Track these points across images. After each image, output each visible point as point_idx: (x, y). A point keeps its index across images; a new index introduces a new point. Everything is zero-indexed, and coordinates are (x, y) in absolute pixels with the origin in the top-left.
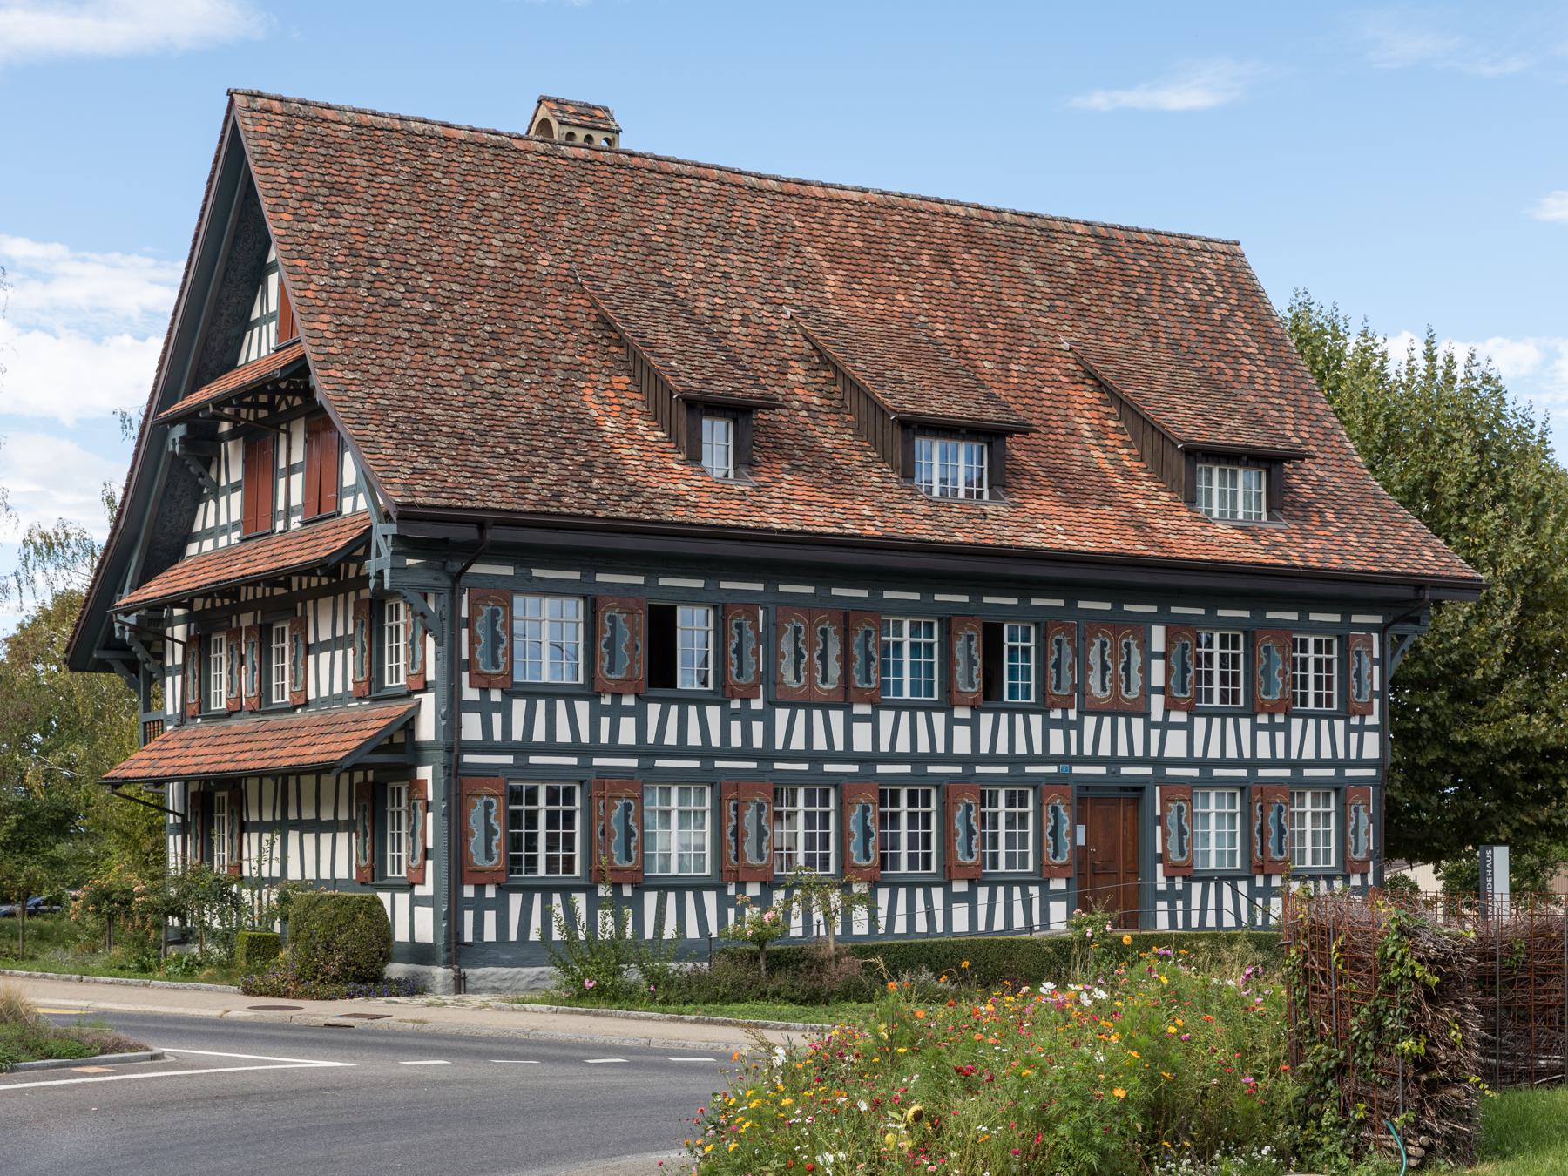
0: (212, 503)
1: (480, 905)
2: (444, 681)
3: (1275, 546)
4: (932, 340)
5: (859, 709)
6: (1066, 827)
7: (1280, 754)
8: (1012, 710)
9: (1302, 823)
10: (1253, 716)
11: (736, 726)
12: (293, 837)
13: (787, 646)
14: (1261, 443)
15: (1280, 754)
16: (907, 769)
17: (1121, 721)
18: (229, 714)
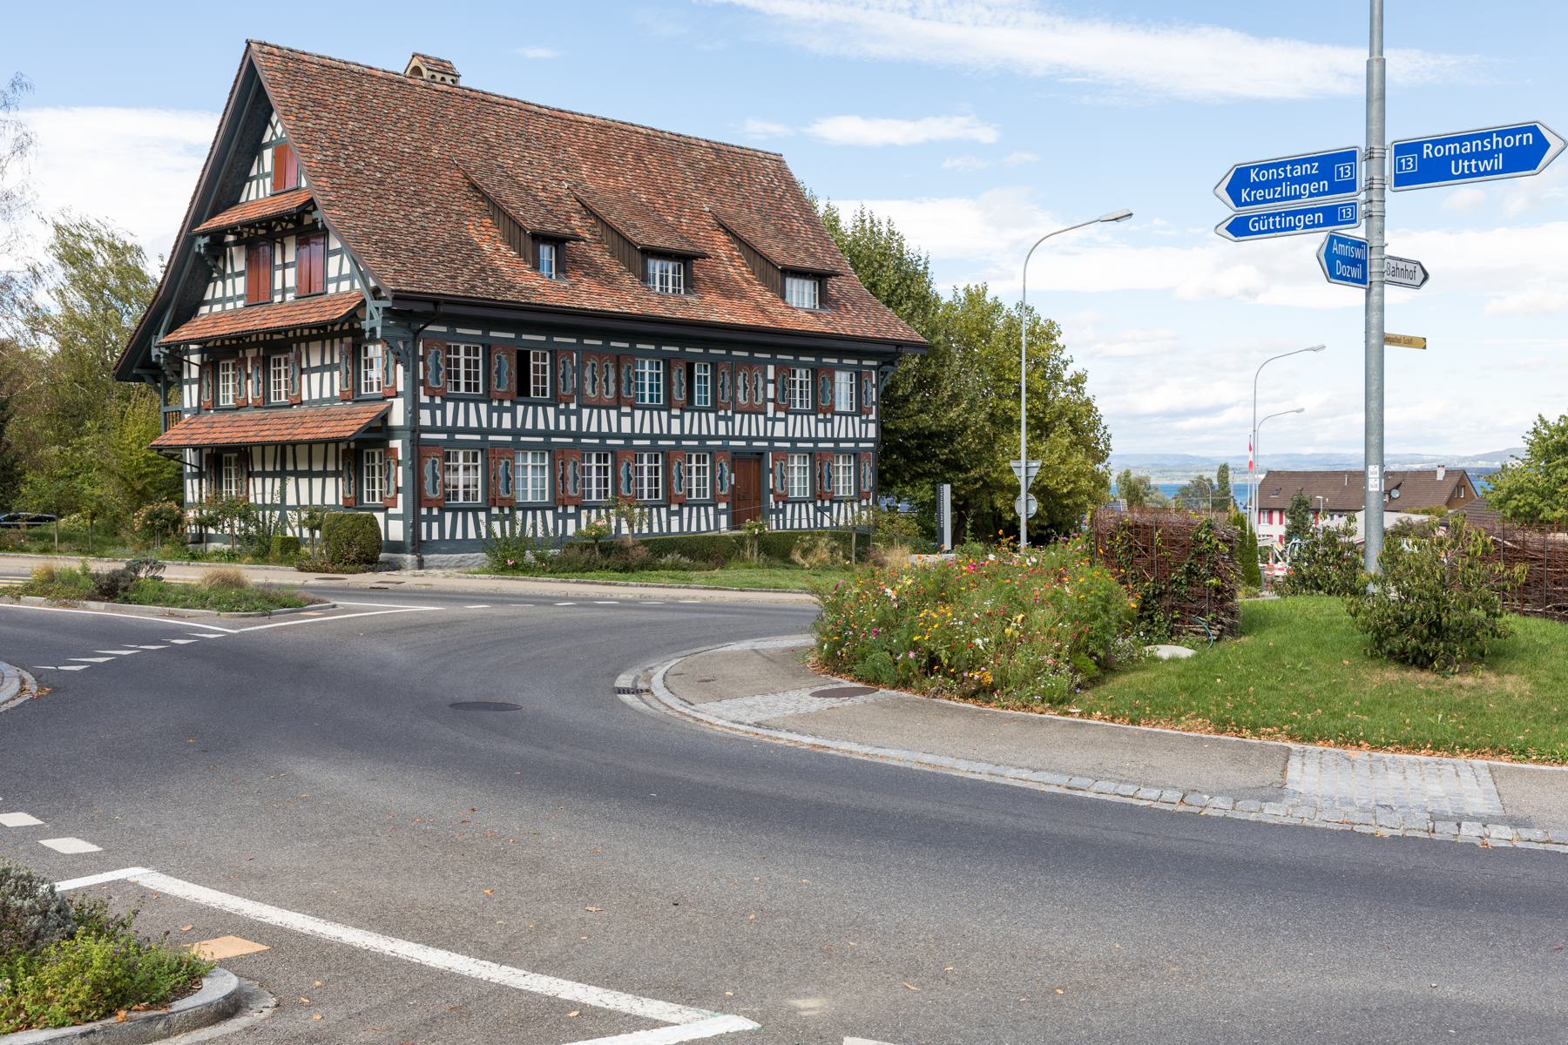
0: (220, 284)
1: (430, 519)
2: (410, 392)
3: (829, 323)
8: (535, 404)
11: (562, 418)
12: (291, 482)
13: (588, 374)
14: (817, 267)
16: (648, 442)
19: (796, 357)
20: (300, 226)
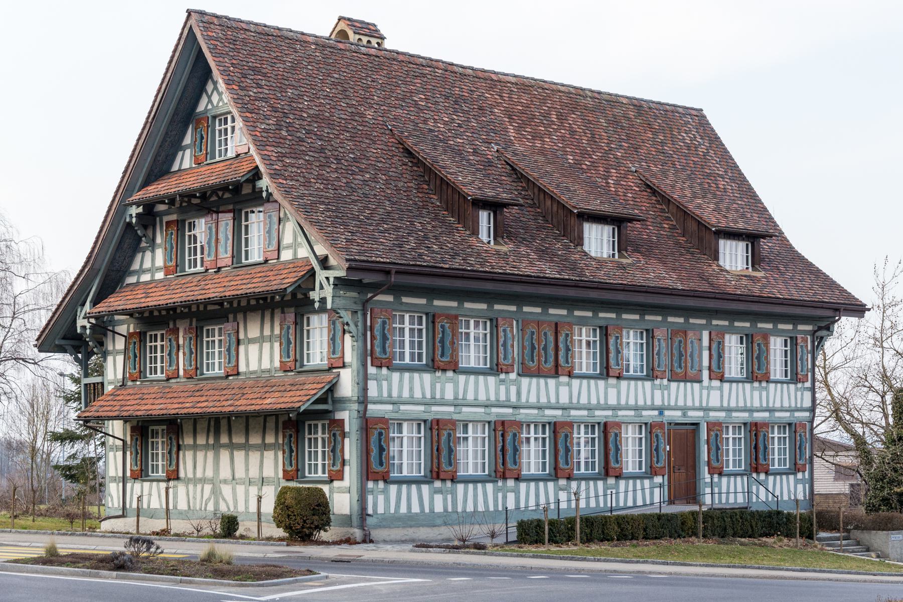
0: (148, 254)
14: (750, 228)
19: (775, 326)
20: (235, 197)
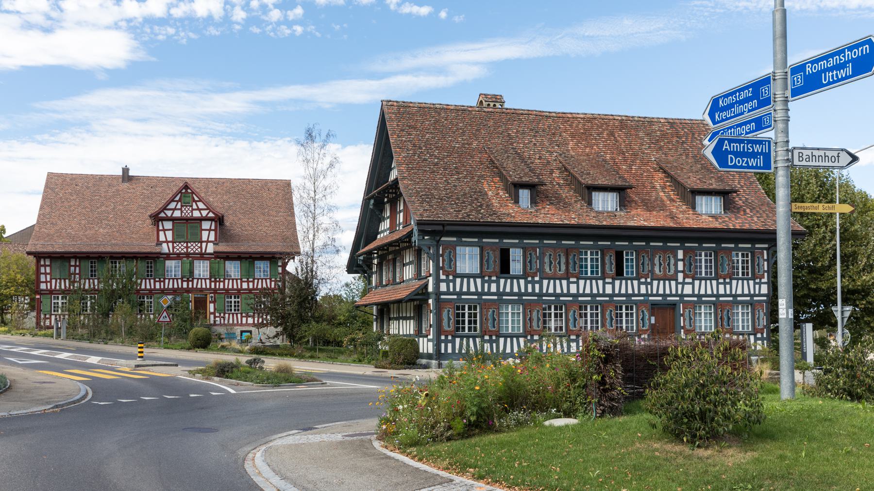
1: (446, 342)
4: (605, 160)
5: (572, 280)
6: (647, 317)
7: (728, 292)
8: (627, 279)
9: (738, 316)
10: (717, 280)
11: (530, 286)
13: (547, 260)
15: (728, 292)
16: (589, 298)
17: (667, 282)
18: (387, 285)
